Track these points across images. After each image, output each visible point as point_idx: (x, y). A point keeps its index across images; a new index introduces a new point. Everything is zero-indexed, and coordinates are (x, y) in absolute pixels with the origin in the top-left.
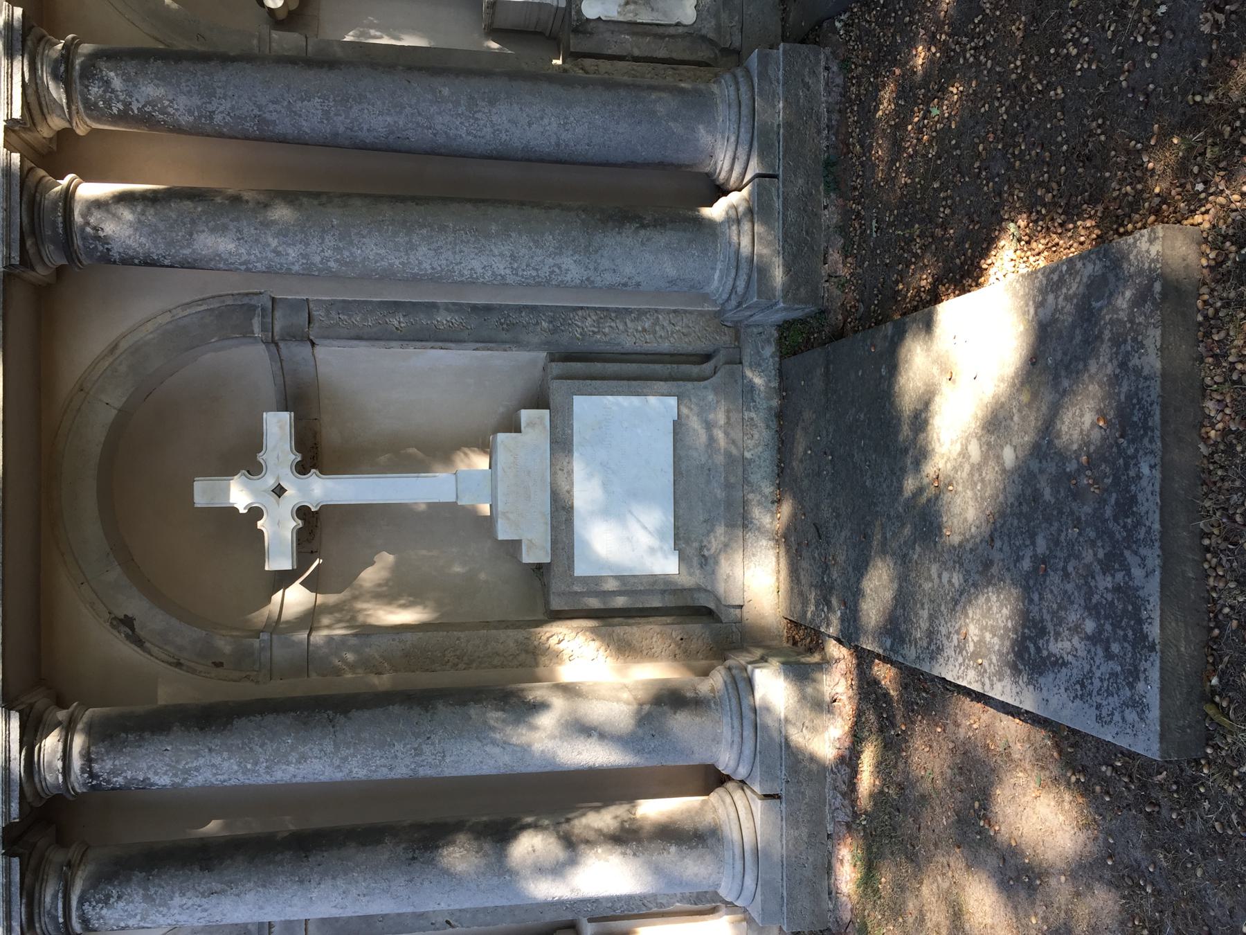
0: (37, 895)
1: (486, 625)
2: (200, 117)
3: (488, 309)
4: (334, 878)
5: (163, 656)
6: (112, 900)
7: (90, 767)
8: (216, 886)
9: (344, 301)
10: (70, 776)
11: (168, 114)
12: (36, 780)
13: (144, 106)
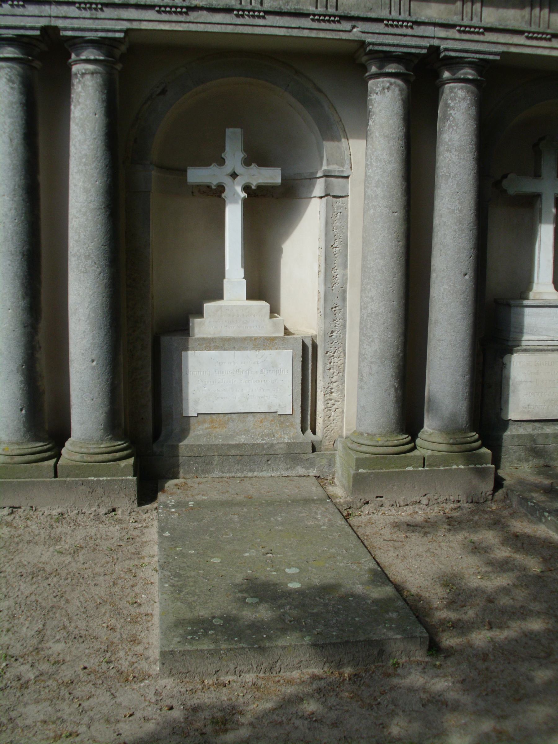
2: (448, 145)
3: (344, 299)
6: (11, 84)
7: (89, 73)
9: (347, 216)
11: (449, 128)
12: (84, 45)
13: (453, 117)
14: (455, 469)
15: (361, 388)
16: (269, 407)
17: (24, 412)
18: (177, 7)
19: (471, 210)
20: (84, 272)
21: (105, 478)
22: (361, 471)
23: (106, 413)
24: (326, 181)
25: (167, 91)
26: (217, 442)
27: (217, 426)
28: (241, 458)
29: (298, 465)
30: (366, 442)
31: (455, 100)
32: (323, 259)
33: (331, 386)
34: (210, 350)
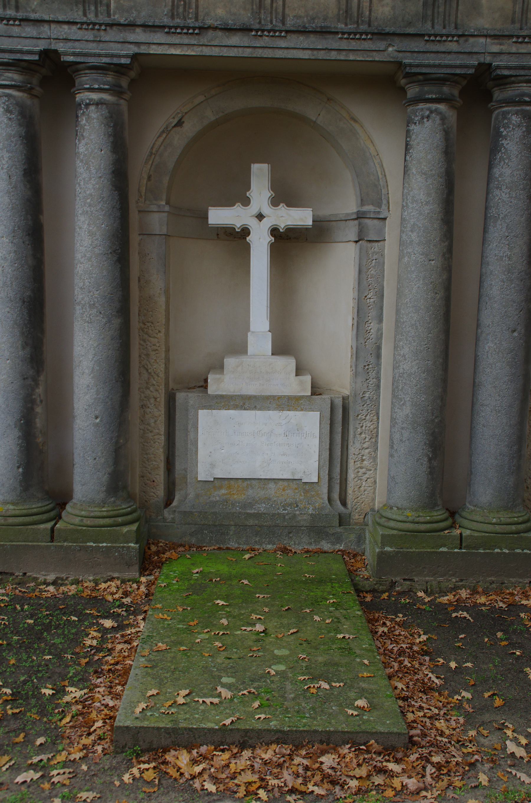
0: (13, 68)
1: (167, 350)
2: (498, 181)
3: (378, 356)
4: (15, 252)
5: (156, 147)
7: (93, 104)
8: (14, 179)
9: (384, 263)
10: (88, 92)
11: (500, 162)
12: (87, 71)
14: (498, 553)
15: (391, 456)
16: (293, 474)
17: (21, 470)
18: (188, 28)
19: (522, 257)
20: (88, 322)
21: (105, 544)
22: (388, 549)
23: (109, 474)
24: (360, 224)
25: (183, 122)
26: (234, 510)
27: (234, 492)
28: (259, 529)
29: (323, 539)
30: (394, 517)
31: (509, 127)
32: (356, 310)
33: (363, 452)
34: (229, 409)
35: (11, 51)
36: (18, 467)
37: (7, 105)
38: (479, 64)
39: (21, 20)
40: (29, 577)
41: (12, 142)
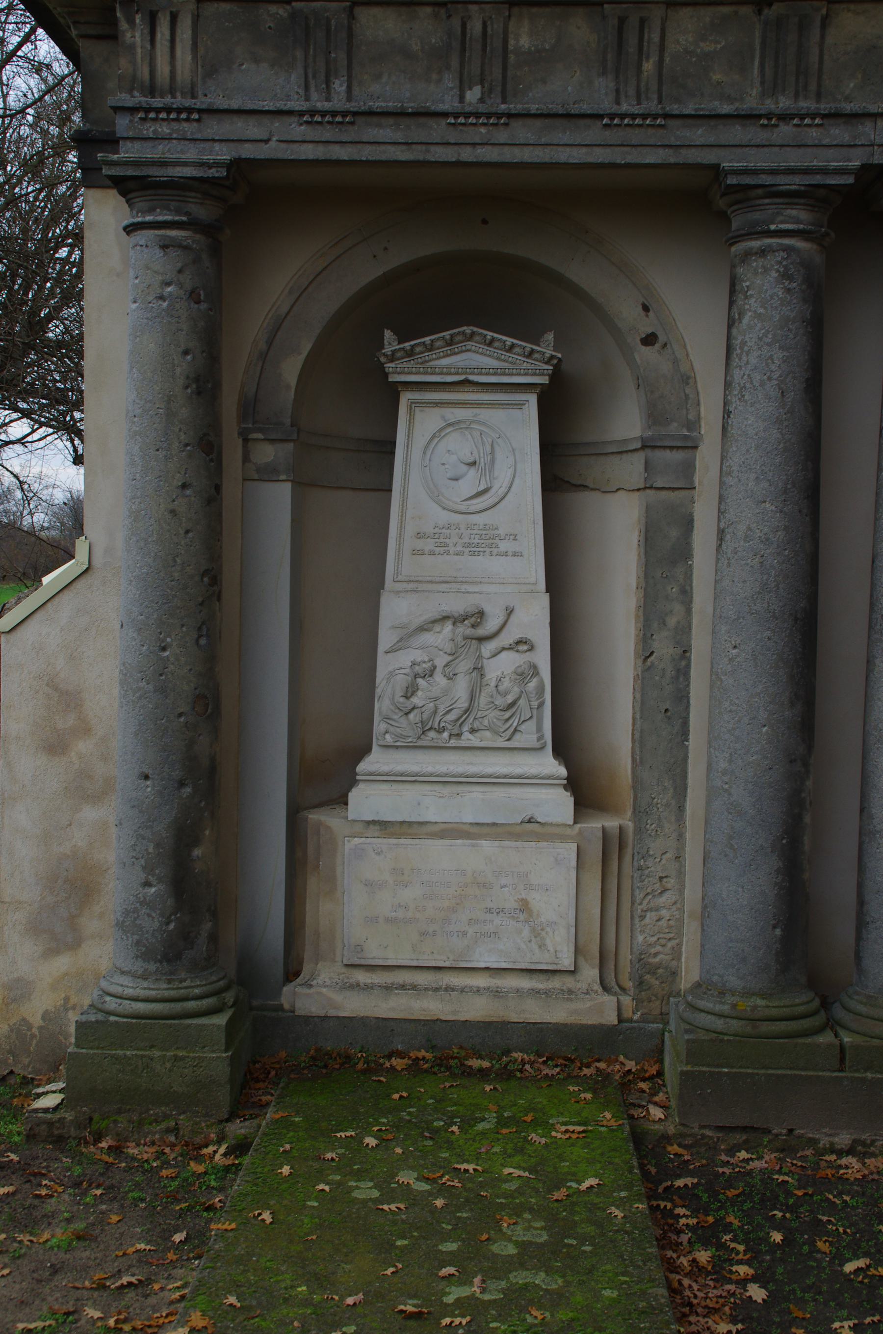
0: (802, 201)
4: (786, 528)
17: (778, 932)
21: (726, 1070)
35: (807, 171)
36: (774, 927)
37: (785, 267)
38: (863, 166)
39: (824, 117)
40: (799, 1137)
41: (790, 330)
